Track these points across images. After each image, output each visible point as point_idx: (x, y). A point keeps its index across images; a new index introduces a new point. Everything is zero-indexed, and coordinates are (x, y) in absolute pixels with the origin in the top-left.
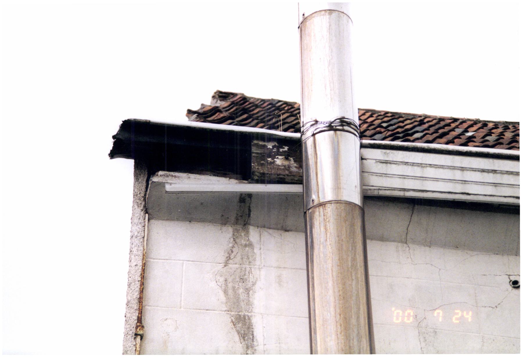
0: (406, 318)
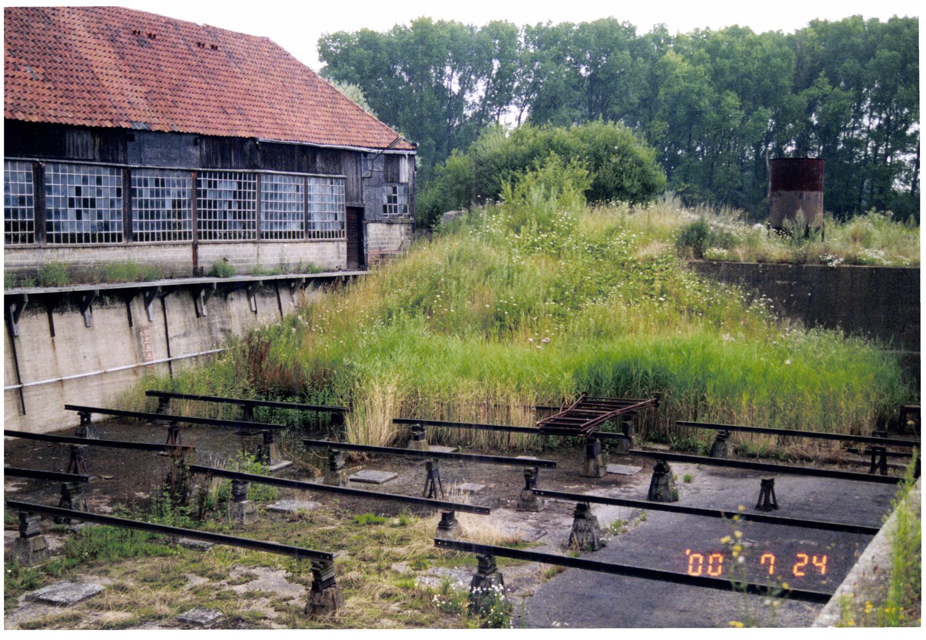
0: (710, 568)
